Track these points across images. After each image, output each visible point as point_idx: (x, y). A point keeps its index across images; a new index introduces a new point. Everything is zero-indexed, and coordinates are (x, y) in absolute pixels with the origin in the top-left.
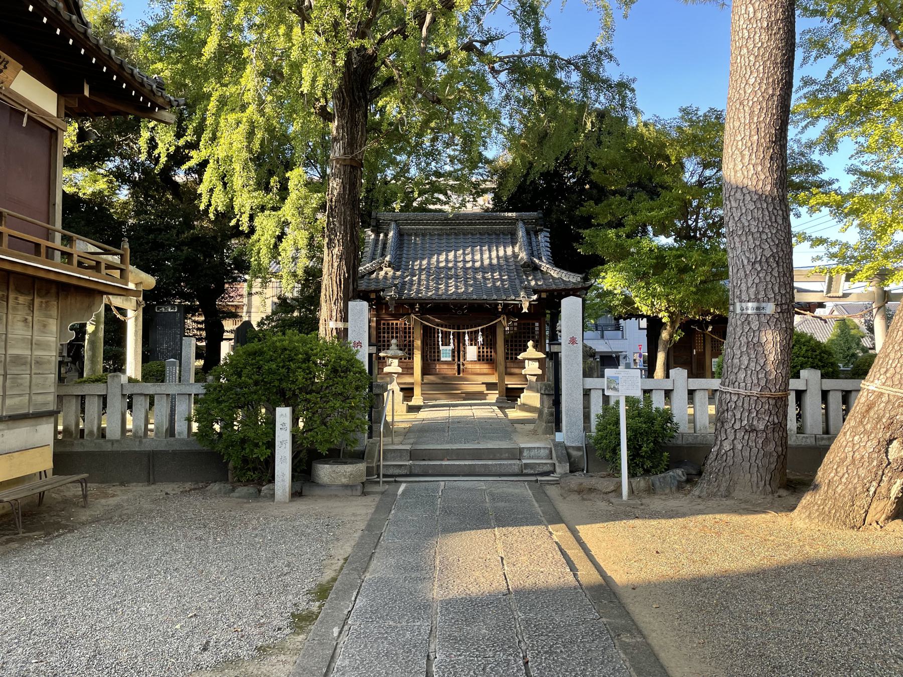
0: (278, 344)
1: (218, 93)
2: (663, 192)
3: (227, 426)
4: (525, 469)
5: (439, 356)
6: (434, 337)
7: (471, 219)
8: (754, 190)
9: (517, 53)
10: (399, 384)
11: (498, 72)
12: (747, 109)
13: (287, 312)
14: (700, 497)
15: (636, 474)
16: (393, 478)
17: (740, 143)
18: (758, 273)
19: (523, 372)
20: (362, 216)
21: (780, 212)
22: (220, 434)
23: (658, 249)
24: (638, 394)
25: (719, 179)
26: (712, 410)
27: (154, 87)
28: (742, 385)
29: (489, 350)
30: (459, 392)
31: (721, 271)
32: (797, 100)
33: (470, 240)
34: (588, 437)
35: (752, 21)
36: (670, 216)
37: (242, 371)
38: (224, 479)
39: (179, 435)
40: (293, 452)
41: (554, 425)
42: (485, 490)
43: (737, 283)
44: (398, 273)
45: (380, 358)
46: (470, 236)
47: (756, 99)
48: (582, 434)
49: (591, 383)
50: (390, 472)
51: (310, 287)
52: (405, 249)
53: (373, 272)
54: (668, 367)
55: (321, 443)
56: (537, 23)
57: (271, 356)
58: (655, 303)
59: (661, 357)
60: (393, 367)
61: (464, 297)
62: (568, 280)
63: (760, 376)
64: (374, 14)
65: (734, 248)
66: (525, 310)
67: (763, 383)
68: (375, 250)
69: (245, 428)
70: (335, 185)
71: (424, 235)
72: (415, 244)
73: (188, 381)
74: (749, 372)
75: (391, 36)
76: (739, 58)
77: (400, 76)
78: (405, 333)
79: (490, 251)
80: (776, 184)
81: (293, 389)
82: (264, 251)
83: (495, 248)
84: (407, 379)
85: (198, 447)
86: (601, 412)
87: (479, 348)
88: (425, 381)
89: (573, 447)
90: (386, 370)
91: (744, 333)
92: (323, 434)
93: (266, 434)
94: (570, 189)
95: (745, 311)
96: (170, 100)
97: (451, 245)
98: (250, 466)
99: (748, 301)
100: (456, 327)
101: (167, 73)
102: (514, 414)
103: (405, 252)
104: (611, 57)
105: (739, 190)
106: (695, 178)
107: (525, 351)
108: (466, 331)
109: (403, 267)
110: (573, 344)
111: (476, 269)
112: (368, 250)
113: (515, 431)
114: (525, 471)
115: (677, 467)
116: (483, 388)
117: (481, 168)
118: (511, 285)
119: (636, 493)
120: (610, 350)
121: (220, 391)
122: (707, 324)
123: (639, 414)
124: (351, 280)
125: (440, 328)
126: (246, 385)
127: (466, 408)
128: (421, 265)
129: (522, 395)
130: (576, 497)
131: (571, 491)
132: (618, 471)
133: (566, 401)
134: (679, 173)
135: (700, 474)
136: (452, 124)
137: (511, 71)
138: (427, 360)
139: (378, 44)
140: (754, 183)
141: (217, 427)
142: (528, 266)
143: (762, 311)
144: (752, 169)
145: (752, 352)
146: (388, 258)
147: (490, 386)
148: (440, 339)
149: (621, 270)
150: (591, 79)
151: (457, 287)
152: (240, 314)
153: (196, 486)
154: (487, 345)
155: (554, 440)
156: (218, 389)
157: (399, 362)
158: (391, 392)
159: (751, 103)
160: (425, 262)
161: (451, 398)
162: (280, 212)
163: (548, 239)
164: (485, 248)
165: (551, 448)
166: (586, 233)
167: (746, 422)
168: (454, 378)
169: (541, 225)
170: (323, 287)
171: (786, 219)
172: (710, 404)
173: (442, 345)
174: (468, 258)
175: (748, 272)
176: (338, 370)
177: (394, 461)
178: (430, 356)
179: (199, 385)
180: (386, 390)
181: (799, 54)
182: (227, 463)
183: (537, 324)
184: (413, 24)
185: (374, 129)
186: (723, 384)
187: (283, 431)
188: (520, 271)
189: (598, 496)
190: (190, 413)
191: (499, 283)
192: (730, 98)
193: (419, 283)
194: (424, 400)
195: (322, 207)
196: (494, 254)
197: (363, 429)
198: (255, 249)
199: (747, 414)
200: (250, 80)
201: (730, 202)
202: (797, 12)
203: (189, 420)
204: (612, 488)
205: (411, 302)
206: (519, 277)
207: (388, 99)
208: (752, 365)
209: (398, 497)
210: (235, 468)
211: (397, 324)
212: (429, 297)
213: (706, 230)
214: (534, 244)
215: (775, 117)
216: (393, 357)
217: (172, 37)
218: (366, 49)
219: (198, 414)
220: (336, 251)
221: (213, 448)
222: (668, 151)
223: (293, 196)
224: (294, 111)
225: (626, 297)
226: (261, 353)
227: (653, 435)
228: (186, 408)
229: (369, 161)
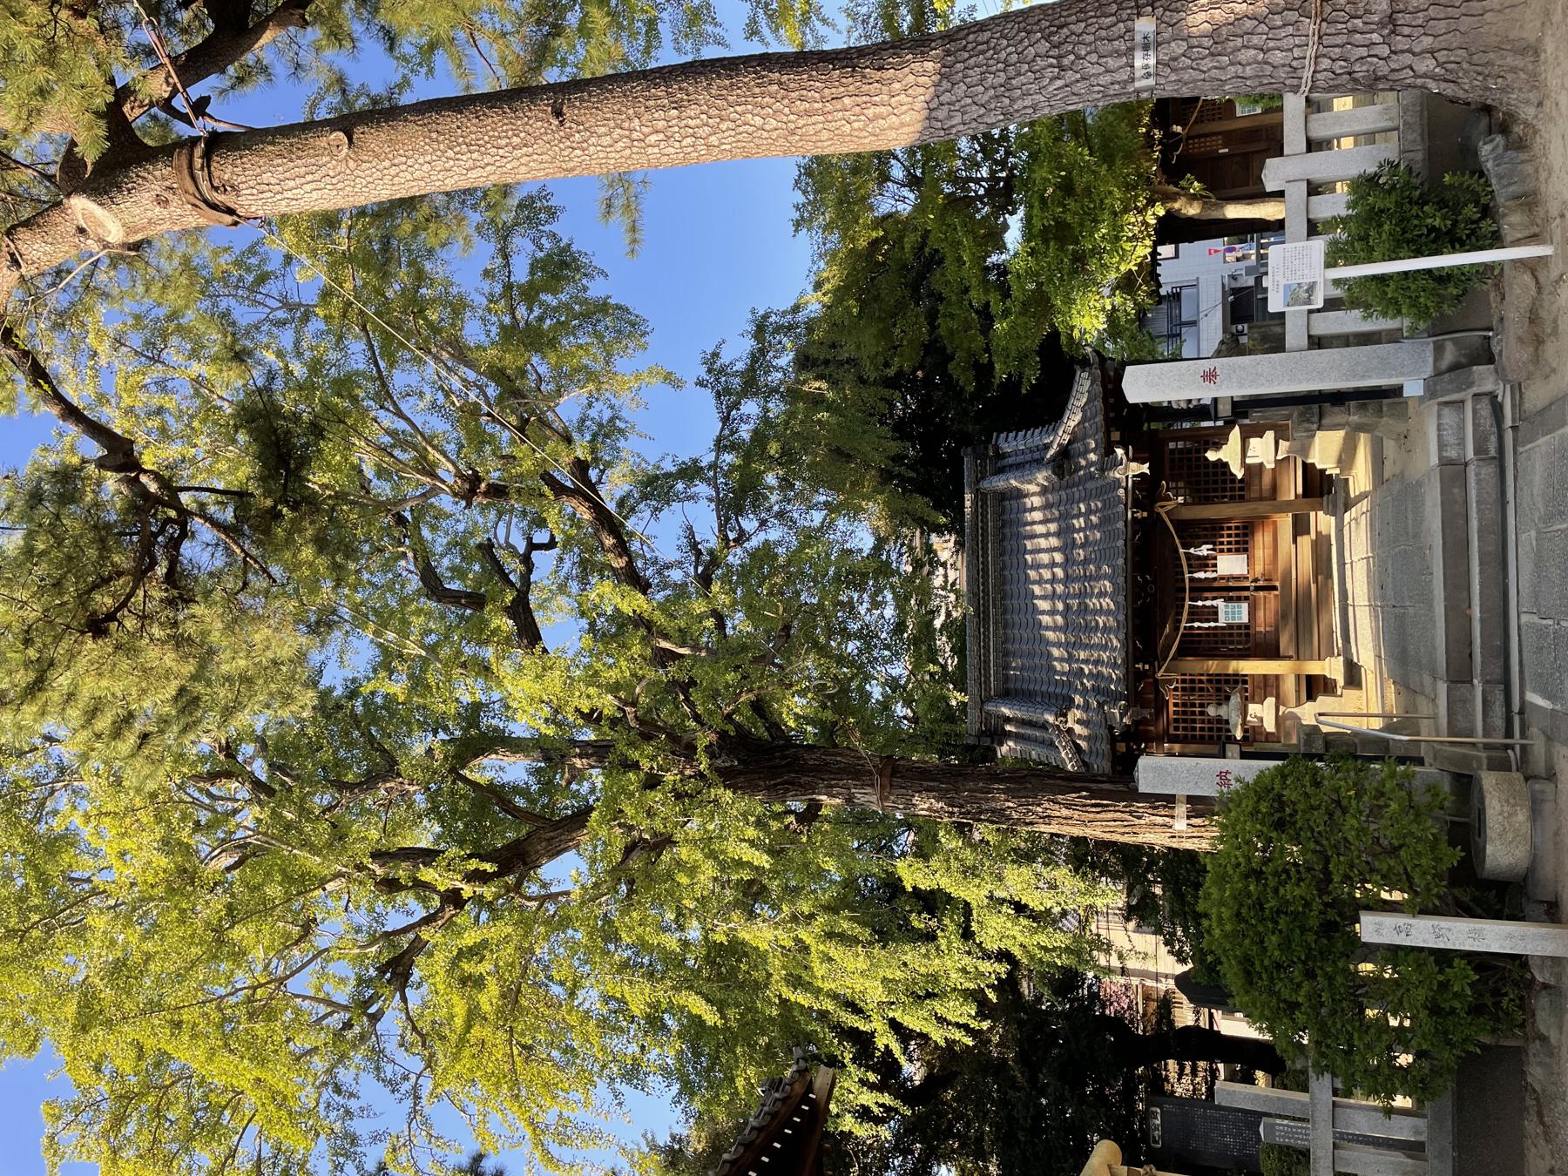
0: (1228, 927)
1: (784, 989)
2: (933, 243)
3: (1401, 1038)
4: (1486, 452)
5: (1239, 626)
6: (1200, 635)
7: (977, 573)
8: (932, 89)
9: (713, 505)
10: (1299, 704)
11: (742, 532)
12: (801, 122)
13: (1156, 909)
14: (1540, 104)
15: (1494, 233)
16: (1513, 717)
17: (856, 125)
18: (1078, 57)
19: (1270, 466)
20: (974, 762)
21: (971, 37)
22: (1419, 1055)
23: (1028, 241)
24: (1319, 245)
25: (911, 152)
26: (1343, 104)
27: (777, 1095)
28: (1297, 53)
29: (1225, 533)
30: (1313, 587)
31: (1072, 124)
32: (783, 43)
34: (1414, 333)
35: (669, 134)
36: (970, 225)
37: (1285, 1001)
38: (1518, 1054)
39: (1421, 1134)
40: (1458, 915)
41: (1385, 401)
42: (1539, 532)
43: (1099, 92)
44: (1078, 699)
45: (1245, 738)
46: (1007, 573)
47: (786, 110)
48: (1406, 345)
49: (1295, 334)
50: (1498, 721)
51: (1106, 861)
52: (1031, 687)
53: (1077, 746)
54: (1262, 196)
55: (1438, 860)
56: (668, 475)
57: (1252, 942)
58: (1130, 234)
59: (1234, 211)
60: (1263, 713)
61: (1121, 580)
62: (1086, 395)
63: (1279, 23)
64: (660, 729)
65: (1035, 107)
66: (1145, 468)
67: (1292, 16)
68: (1035, 741)
69: (1406, 1005)
70: (924, 805)
71: (1006, 654)
72: (1021, 669)
73: (1303, 1104)
74: (1271, 44)
75: (692, 705)
76: (723, 147)
77: (750, 690)
78: (1193, 689)
79: (1033, 536)
80: (922, 53)
81: (1321, 907)
82: (1042, 939)
83: (1028, 528)
84: (1289, 686)
85: (1447, 1101)
86: (1357, 313)
87: (1222, 551)
88: (1291, 653)
89: (1436, 360)
90: (1270, 726)
91: (1194, 65)
92: (1419, 854)
93: (1419, 967)
94: (922, 404)
95: (1151, 70)
96: (797, 1071)
97: (1023, 606)
98: (1489, 1001)
99: (1132, 67)
100: (1180, 595)
101: (751, 1071)
102: (1360, 479)
103: (1037, 688)
104: (715, 355)
105: (934, 114)
106: (905, 192)
107: (1226, 465)
108: (1187, 576)
109: (1064, 692)
110: (1215, 376)
111: (1067, 560)
112: (1034, 753)
113: (1401, 476)
114: (1493, 453)
115: (1475, 153)
116: (1305, 542)
117: (889, 556)
118: (1097, 497)
119: (1536, 230)
120: (1220, 307)
121: (1328, 1046)
122: (1168, 134)
123: (1361, 239)
124: (1094, 786)
125: (1183, 624)
126: (1314, 995)
127: (1348, 573)
128: (1061, 660)
129: (1319, 466)
130: (1550, 348)
131: (1536, 359)
132: (1488, 267)
133: (1335, 380)
134: (897, 222)
135: (1487, 109)
136: (821, 606)
137: (740, 511)
139: (703, 725)
140: (921, 90)
141: (1405, 1059)
142: (1061, 467)
143: (1151, 39)
144: (897, 98)
145: (1231, 44)
146: (1050, 718)
147: (1300, 527)
148: (1206, 625)
149: (1069, 302)
150: (751, 383)
151: (1102, 594)
152: (1162, 994)
153: (1533, 1111)
154: (1215, 536)
155: (1421, 399)
156: (1324, 1049)
157: (1253, 702)
158: (1322, 718)
159: (792, 117)
160: (1056, 652)
162: (974, 905)
163: (1012, 435)
164: (1029, 545)
165: (1440, 404)
166: (1001, 373)
167: (1375, 36)
169: (986, 449)
170: (1107, 837)
171: (981, 26)
172: (1330, 108)
173: (1216, 620)
174: (1047, 574)
175: (1078, 76)
176: (1280, 818)
177: (1473, 715)
178: (1239, 643)
179: (1313, 1084)
180: (1315, 729)
181: (710, 52)
182: (1483, 1047)
183: (1172, 445)
184: (672, 668)
185: (831, 735)
186: (1295, 89)
187: (1413, 931)
188: (1071, 482)
189: (1546, 304)
190: (1375, 1109)
191: (1093, 518)
192: (784, 152)
193: (1097, 662)
194: (1332, 655)
195: (962, 829)
196: (1040, 529)
197: (1405, 775)
198: (1039, 954)
199: (1358, 36)
200: (761, 934)
201: (953, 126)
202: (653, 65)
203: (1390, 1112)
204: (1527, 278)
205: (1133, 678)
206: (1082, 481)
207: (785, 710)
208: (1255, 40)
209: (1558, 707)
210: (1494, 1031)
211: (1176, 705)
212: (1123, 646)
213: (996, 162)
214: (1020, 459)
215: (814, 73)
216: (1245, 713)
217: (697, 1054)
218: (711, 744)
219: (1377, 1093)
221: (1449, 1070)
222: (862, 243)
223: (946, 883)
224: (806, 865)
225: (1118, 287)
226: (1246, 963)
227: (1407, 207)
228: (1363, 1112)
229: (885, 746)
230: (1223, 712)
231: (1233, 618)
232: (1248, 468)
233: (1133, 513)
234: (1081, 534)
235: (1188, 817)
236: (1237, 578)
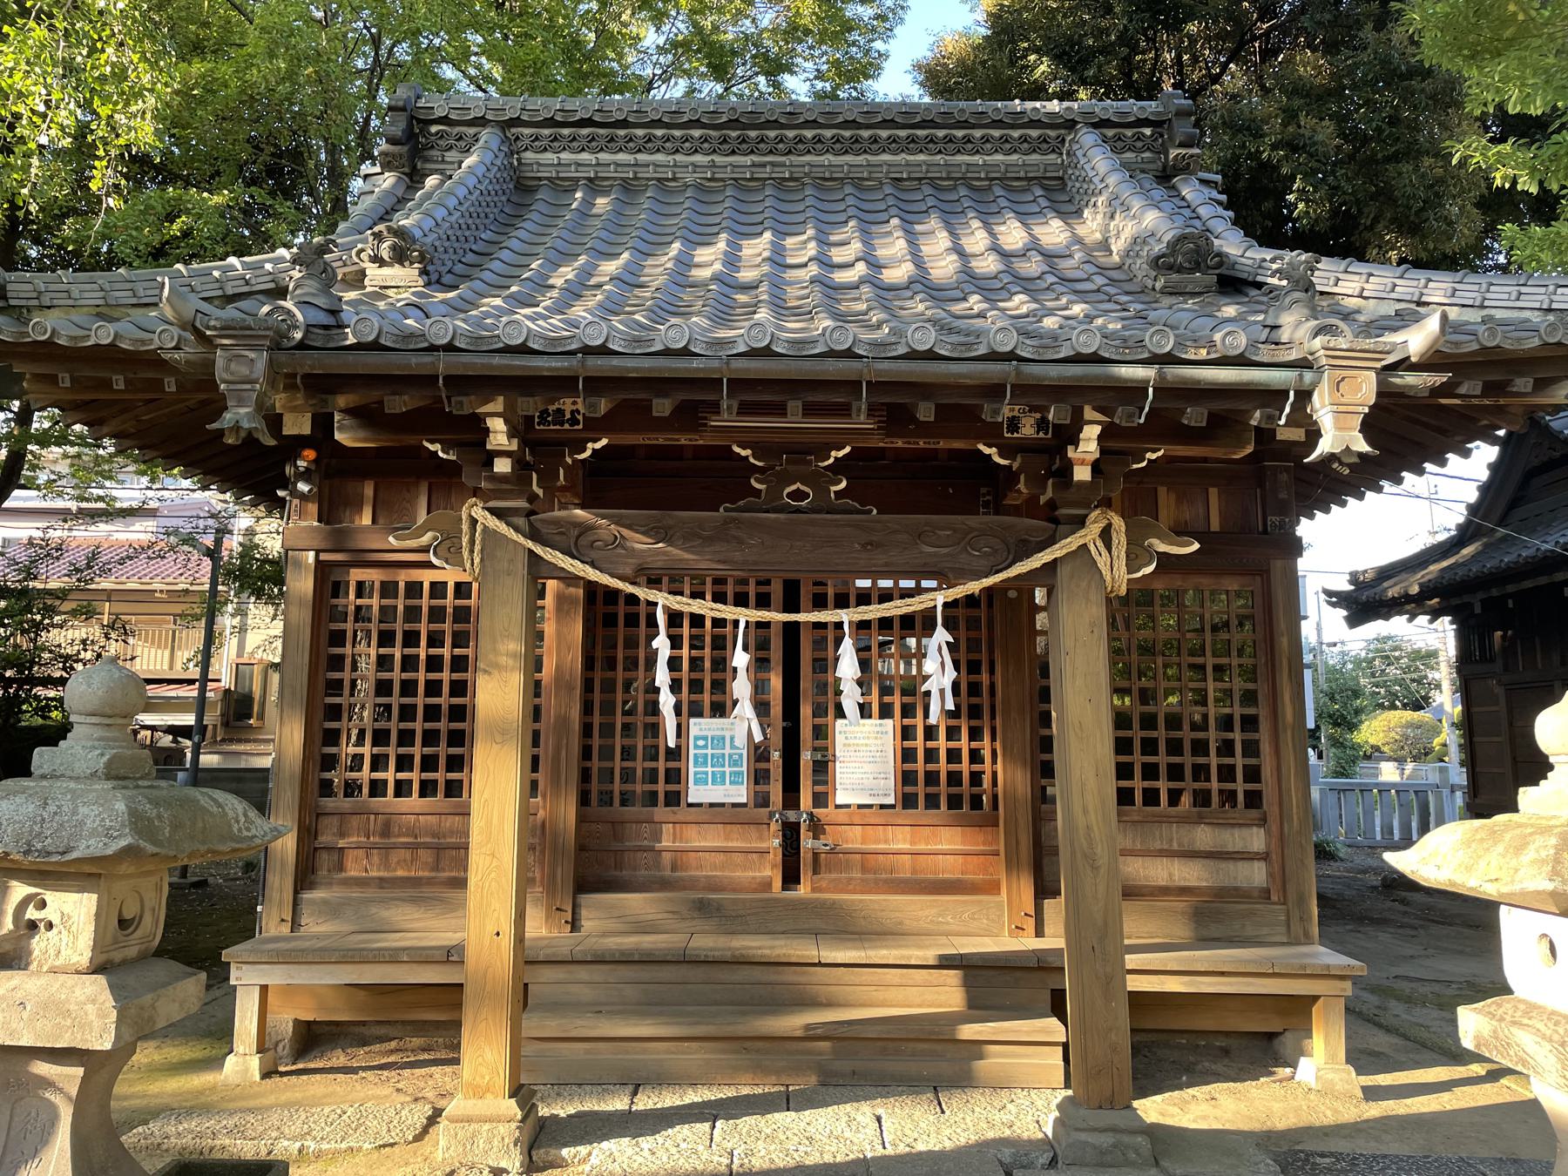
5: (675, 776)
33: (850, 201)
72: (585, 213)
116: (947, 994)
125: (663, 600)
138: (606, 798)
148: (662, 677)
231: (702, 761)
236: (823, 768)
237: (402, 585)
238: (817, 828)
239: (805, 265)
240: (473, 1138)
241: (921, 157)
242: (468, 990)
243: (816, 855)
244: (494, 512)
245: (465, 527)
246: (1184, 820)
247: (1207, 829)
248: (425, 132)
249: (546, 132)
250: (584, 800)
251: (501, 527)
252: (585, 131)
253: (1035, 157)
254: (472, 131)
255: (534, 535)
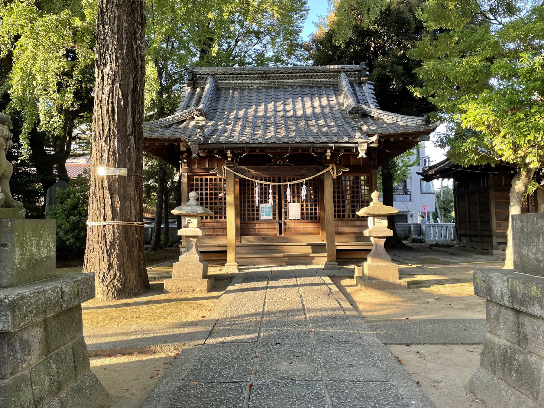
5: (258, 215)
29: (313, 207)
33: (291, 92)
53: (183, 121)
62: (405, 124)
71: (242, 89)
72: (233, 97)
87: (302, 205)
108: (288, 183)
109: (217, 116)
111: (298, 117)
116: (308, 250)
124: (129, 110)
138: (245, 219)
142: (357, 112)
147: (317, 248)
151: (276, 133)
161: (271, 263)
168: (275, 239)
178: (249, 215)
214: (358, 94)
216: (191, 216)
220: (107, 69)
230: (192, 202)
232: (364, 219)
233: (331, 147)
234: (314, 123)
235: (108, 177)
236: (286, 213)
237: (204, 179)
238: (285, 224)
239: (280, 111)
240: (230, 268)
241: (307, 80)
242: (228, 246)
243: (285, 229)
244: (228, 167)
245: (223, 170)
246: (352, 220)
247: (359, 222)
248: (195, 77)
249: (223, 76)
250: (241, 220)
251: (230, 170)
252: (231, 76)
253: (332, 79)
254: (206, 76)
255: (235, 171)
